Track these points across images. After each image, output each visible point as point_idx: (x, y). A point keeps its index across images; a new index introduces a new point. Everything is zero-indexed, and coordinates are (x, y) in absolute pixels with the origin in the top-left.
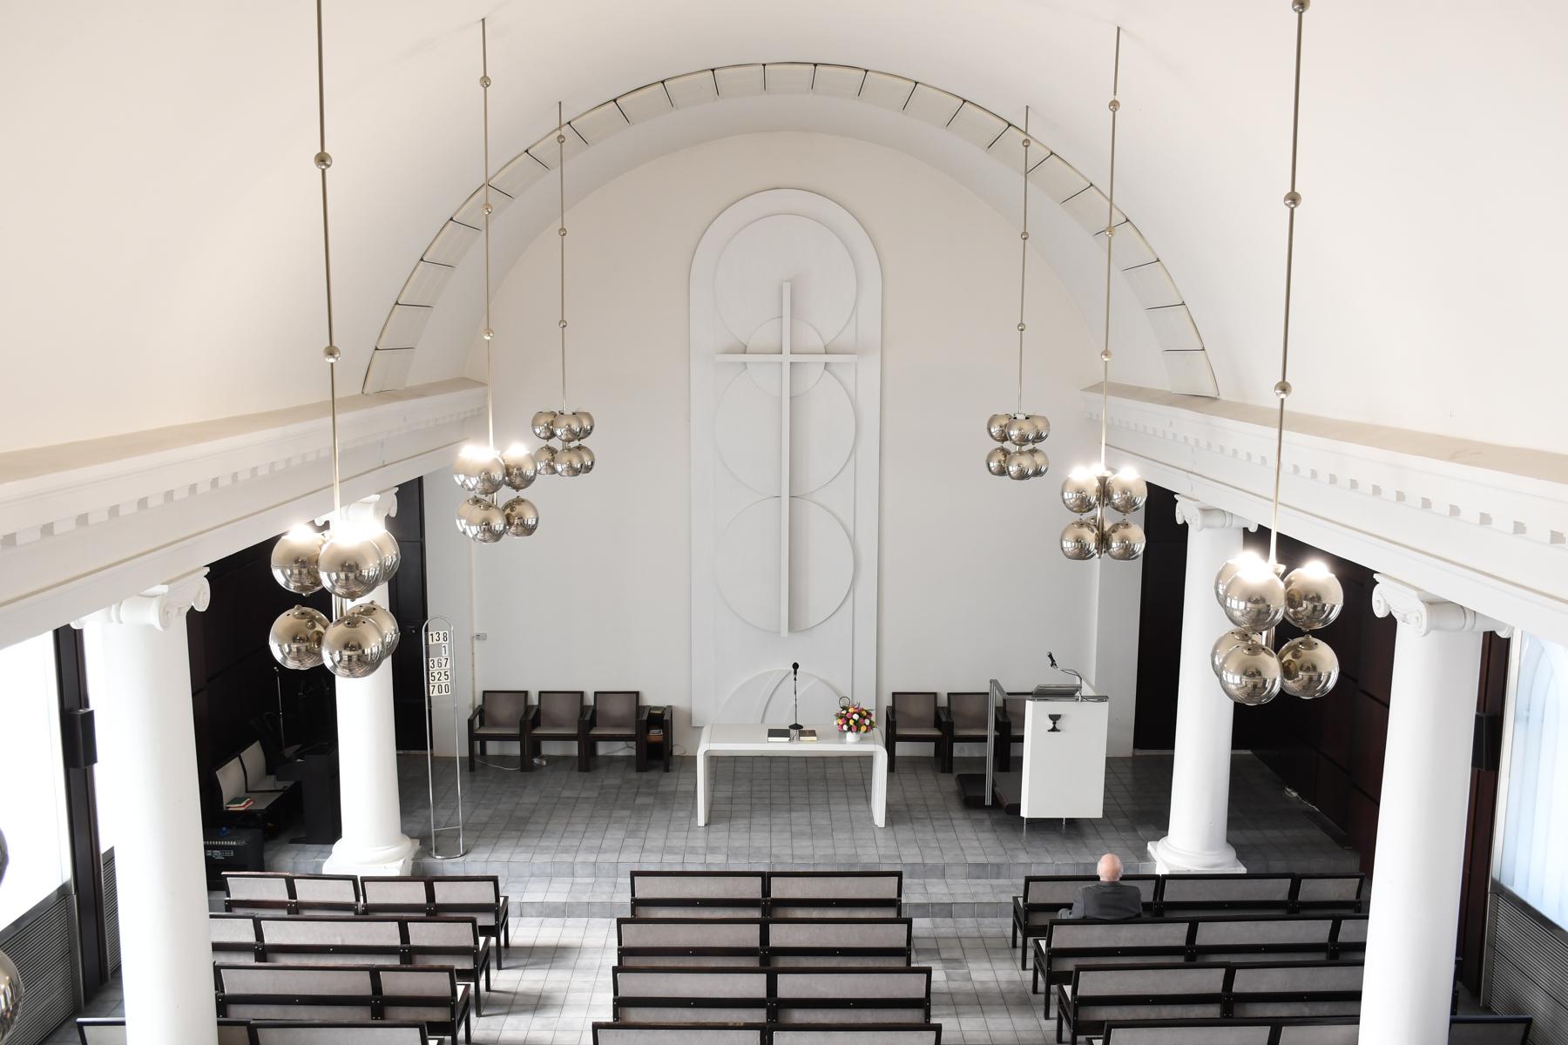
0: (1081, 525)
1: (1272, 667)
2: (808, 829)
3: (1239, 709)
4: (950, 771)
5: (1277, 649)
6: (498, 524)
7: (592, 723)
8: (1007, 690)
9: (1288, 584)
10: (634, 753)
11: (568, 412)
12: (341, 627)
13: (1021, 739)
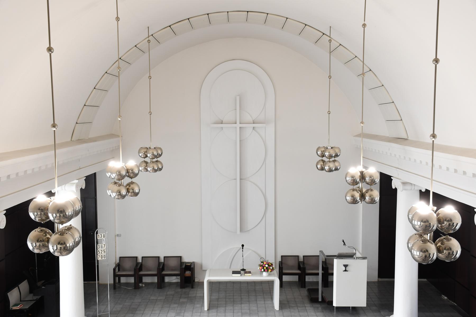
0: (354, 190)
1: (432, 249)
2: (248, 311)
3: (420, 266)
4: (305, 287)
5: (434, 240)
6: (124, 192)
7: (163, 269)
8: (326, 254)
9: (438, 215)
10: (179, 281)
11: (152, 147)
12: (57, 236)
13: (332, 274)
